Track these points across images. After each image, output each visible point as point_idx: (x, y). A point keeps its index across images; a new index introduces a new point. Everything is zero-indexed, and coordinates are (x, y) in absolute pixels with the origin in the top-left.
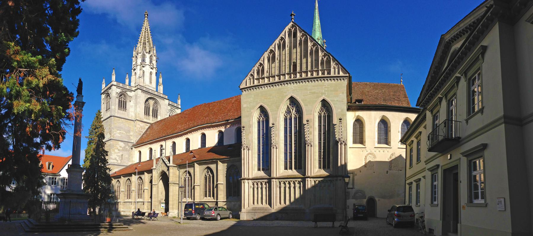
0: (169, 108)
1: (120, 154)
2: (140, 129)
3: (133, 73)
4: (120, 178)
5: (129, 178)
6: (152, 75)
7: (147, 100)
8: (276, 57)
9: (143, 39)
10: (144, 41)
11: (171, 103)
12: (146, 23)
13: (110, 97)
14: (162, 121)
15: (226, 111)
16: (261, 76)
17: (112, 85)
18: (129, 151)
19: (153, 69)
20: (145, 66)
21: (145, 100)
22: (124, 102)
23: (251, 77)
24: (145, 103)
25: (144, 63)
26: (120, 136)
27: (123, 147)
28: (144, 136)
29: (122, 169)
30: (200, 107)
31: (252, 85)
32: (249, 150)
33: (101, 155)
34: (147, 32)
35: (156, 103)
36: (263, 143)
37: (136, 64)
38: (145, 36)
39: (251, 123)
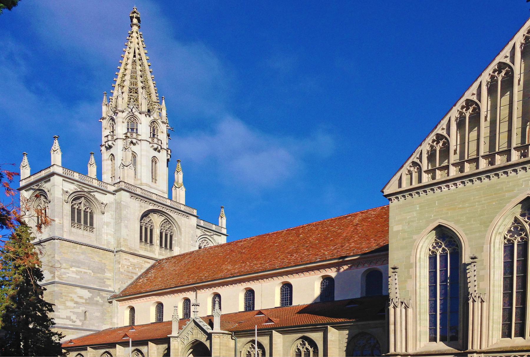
0: (199, 232)
1: (81, 309)
2: (131, 268)
3: (106, 155)
4: (86, 349)
5: (107, 350)
6: (158, 164)
7: (146, 215)
8: (452, 148)
9: (128, 78)
10: (132, 77)
11: (202, 223)
12: (135, 40)
13: (46, 198)
14: (184, 257)
15: (340, 240)
16: (441, 162)
17: (53, 174)
18: (102, 305)
19: (159, 151)
20: (139, 142)
21: (141, 214)
22: (85, 212)
23: (412, 169)
24: (141, 220)
25: (134, 135)
26: (78, 277)
27: (87, 297)
28: (141, 280)
29: (88, 336)
30: (277, 236)
31: (415, 184)
32: (406, 307)
33: (34, 310)
34: (138, 63)
35: (168, 220)
36: (444, 295)
37: (113, 136)
38: (134, 72)
39: (412, 260)
